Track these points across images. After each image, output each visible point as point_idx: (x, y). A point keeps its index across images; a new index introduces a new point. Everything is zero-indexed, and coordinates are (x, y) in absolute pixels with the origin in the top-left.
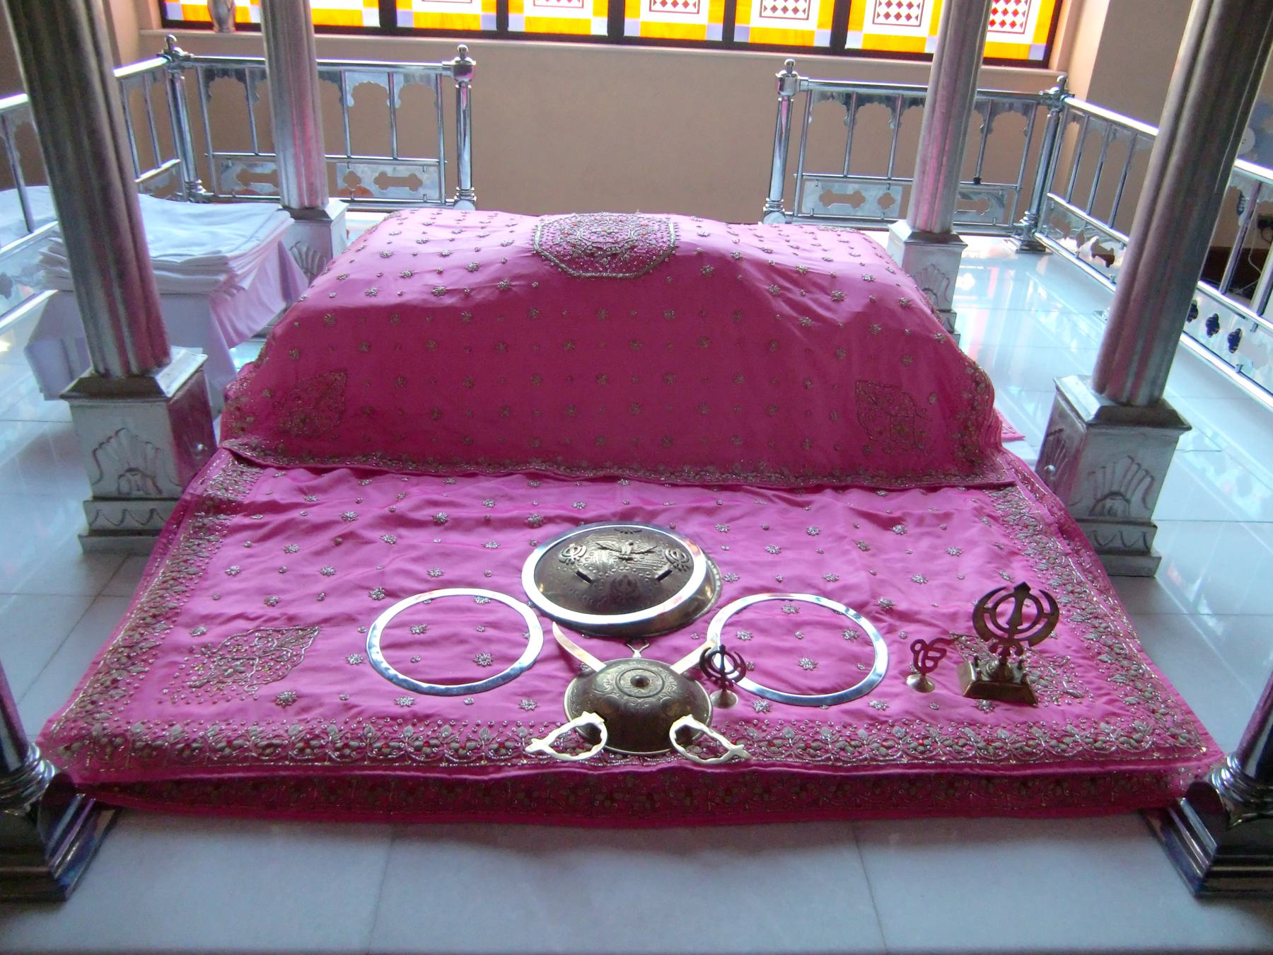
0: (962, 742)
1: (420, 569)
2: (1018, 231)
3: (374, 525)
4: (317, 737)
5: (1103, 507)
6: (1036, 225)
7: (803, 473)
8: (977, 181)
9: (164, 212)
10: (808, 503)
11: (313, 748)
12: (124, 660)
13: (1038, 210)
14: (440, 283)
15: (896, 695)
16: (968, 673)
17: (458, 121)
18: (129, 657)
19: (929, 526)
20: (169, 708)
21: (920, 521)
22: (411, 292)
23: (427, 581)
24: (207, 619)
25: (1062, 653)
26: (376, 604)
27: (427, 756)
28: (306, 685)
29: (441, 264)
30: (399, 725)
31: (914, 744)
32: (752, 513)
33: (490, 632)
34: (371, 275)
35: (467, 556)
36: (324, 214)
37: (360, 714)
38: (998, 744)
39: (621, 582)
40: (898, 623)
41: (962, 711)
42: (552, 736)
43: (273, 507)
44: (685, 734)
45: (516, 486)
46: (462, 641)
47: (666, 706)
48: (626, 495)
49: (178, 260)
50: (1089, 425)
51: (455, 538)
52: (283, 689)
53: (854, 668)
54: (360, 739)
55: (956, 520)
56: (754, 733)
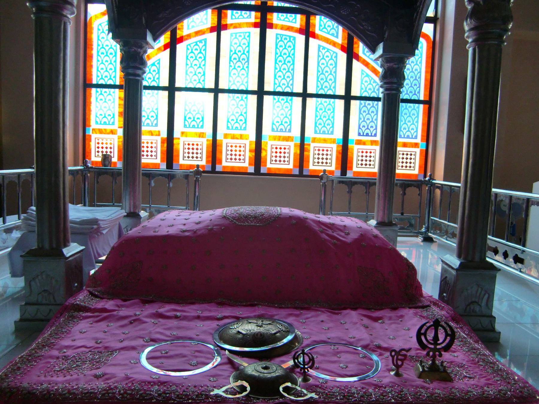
0: (419, 394)
1: (168, 333)
2: (421, 233)
3: (147, 317)
4: (112, 389)
5: (470, 308)
6: (428, 231)
7: (336, 303)
8: (402, 214)
9: (74, 209)
10: (340, 313)
11: (109, 394)
12: (25, 360)
13: (428, 225)
14: (184, 228)
15: (386, 377)
16: (418, 369)
17: (195, 200)
18: (28, 359)
19: (395, 320)
20: (43, 378)
21: (390, 318)
22: (172, 231)
23: (169, 337)
24: (67, 347)
25: (461, 362)
26: (146, 344)
27: (164, 398)
28: (109, 370)
29: (185, 222)
30: (152, 385)
31: (396, 394)
32: (317, 316)
33: (197, 354)
34: (157, 225)
35: (188, 329)
36: (139, 215)
37: (133, 380)
38: (436, 395)
39: (257, 334)
40: (384, 352)
41: (418, 383)
42: (224, 389)
43: (104, 310)
44: (286, 389)
45: (213, 307)
46: (185, 356)
47: (277, 377)
48: (260, 310)
49: (78, 220)
50: (457, 270)
51: (184, 323)
52: (99, 372)
53: (365, 367)
54: (132, 390)
55: (406, 318)
56: (319, 390)
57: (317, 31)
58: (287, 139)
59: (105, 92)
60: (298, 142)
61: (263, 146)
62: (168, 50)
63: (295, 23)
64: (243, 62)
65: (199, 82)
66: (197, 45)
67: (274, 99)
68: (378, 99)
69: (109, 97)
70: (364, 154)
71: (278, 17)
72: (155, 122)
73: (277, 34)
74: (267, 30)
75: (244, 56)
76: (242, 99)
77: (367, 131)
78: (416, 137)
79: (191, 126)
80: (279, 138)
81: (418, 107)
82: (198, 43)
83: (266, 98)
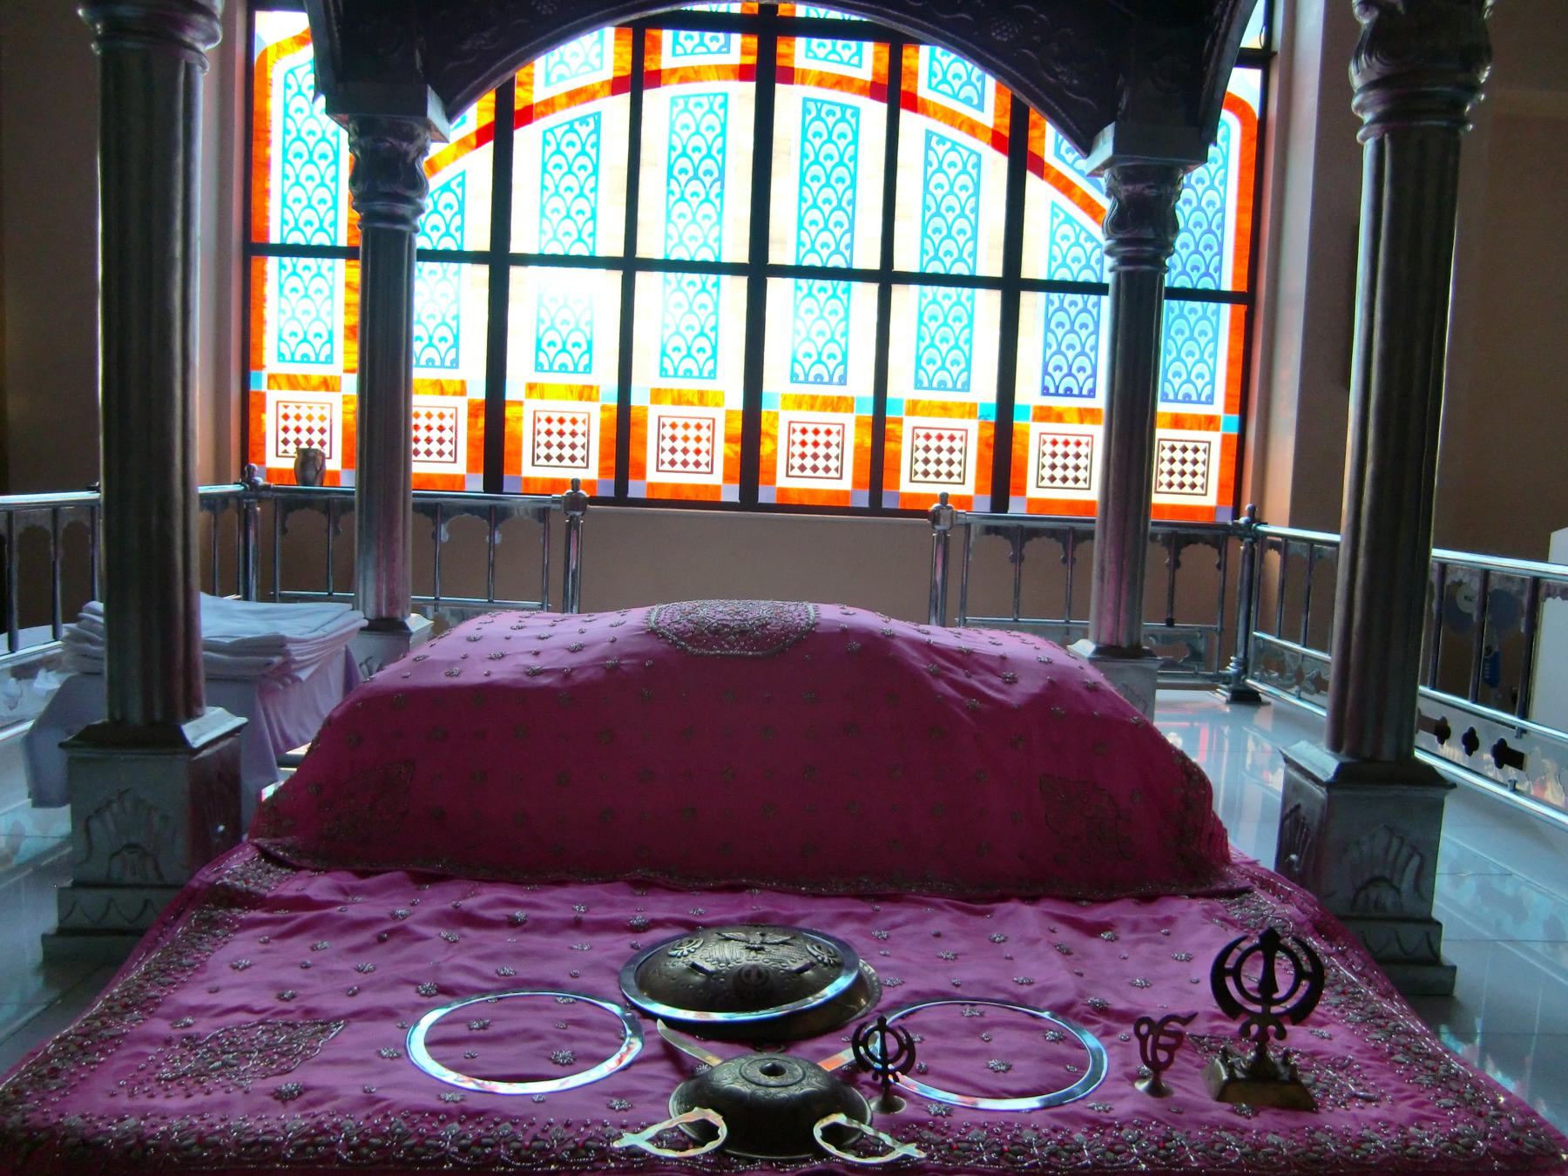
0: (1218, 1146)
1: (488, 968)
2: (1226, 679)
3: (426, 922)
4: (325, 1132)
5: (1368, 897)
6: (1245, 671)
7: (979, 882)
8: (1170, 623)
9: (217, 608)
10: (990, 912)
11: (316, 1146)
12: (73, 1048)
13: (1246, 654)
14: (536, 663)
15: (1122, 1097)
16: (1217, 1073)
17: (566, 581)
18: (81, 1046)
19: (1148, 931)
20: (124, 1101)
21: (1135, 927)
22: (501, 672)
23: (493, 980)
24: (195, 1010)
25: (1341, 1053)
26: (425, 1000)
27: (476, 1158)
28: (318, 1077)
29: (538, 645)
30: (442, 1122)
31: (1153, 1147)
32: (922, 920)
33: (572, 1030)
34: (456, 656)
35: (546, 957)
36: (404, 626)
37: (388, 1107)
38: (1269, 1150)
39: (748, 973)
40: (1116, 1025)
41: (1216, 1114)
42: (652, 1131)
43: (304, 903)
44: (833, 1133)
45: (621, 895)
46: (537, 1037)
47: (807, 1098)
48: (756, 904)
49: (227, 641)
50: (1329, 785)
51: (536, 941)
52: (287, 1083)
53: (1061, 1070)
54: (385, 1136)
55: (1181, 925)
56: (927, 1134)
57: (923, 92)
58: (835, 404)
59: (307, 268)
60: (868, 412)
61: (765, 426)
62: (490, 146)
63: (859, 66)
64: (708, 180)
65: (580, 239)
66: (572, 130)
67: (798, 288)
68: (1098, 289)
69: (318, 283)
70: (1060, 449)
71: (809, 49)
72: (452, 355)
73: (806, 100)
74: (778, 86)
75: (709, 164)
76: (704, 289)
77: (1069, 382)
78: (1210, 400)
79: (556, 367)
80: (812, 403)
81: (1217, 313)
82: (577, 125)
83: (774, 285)
